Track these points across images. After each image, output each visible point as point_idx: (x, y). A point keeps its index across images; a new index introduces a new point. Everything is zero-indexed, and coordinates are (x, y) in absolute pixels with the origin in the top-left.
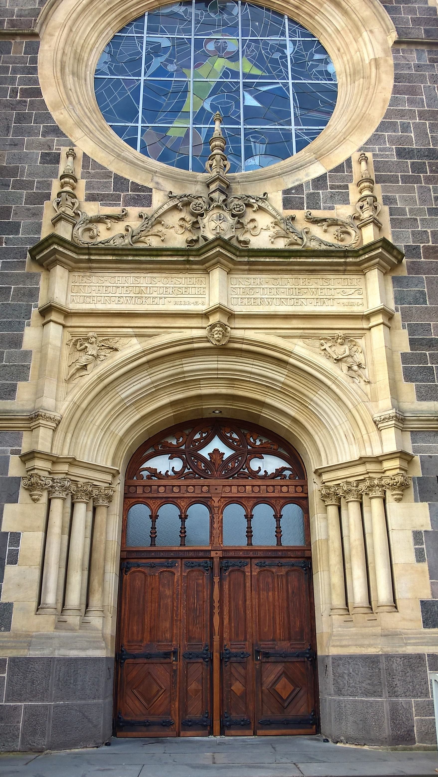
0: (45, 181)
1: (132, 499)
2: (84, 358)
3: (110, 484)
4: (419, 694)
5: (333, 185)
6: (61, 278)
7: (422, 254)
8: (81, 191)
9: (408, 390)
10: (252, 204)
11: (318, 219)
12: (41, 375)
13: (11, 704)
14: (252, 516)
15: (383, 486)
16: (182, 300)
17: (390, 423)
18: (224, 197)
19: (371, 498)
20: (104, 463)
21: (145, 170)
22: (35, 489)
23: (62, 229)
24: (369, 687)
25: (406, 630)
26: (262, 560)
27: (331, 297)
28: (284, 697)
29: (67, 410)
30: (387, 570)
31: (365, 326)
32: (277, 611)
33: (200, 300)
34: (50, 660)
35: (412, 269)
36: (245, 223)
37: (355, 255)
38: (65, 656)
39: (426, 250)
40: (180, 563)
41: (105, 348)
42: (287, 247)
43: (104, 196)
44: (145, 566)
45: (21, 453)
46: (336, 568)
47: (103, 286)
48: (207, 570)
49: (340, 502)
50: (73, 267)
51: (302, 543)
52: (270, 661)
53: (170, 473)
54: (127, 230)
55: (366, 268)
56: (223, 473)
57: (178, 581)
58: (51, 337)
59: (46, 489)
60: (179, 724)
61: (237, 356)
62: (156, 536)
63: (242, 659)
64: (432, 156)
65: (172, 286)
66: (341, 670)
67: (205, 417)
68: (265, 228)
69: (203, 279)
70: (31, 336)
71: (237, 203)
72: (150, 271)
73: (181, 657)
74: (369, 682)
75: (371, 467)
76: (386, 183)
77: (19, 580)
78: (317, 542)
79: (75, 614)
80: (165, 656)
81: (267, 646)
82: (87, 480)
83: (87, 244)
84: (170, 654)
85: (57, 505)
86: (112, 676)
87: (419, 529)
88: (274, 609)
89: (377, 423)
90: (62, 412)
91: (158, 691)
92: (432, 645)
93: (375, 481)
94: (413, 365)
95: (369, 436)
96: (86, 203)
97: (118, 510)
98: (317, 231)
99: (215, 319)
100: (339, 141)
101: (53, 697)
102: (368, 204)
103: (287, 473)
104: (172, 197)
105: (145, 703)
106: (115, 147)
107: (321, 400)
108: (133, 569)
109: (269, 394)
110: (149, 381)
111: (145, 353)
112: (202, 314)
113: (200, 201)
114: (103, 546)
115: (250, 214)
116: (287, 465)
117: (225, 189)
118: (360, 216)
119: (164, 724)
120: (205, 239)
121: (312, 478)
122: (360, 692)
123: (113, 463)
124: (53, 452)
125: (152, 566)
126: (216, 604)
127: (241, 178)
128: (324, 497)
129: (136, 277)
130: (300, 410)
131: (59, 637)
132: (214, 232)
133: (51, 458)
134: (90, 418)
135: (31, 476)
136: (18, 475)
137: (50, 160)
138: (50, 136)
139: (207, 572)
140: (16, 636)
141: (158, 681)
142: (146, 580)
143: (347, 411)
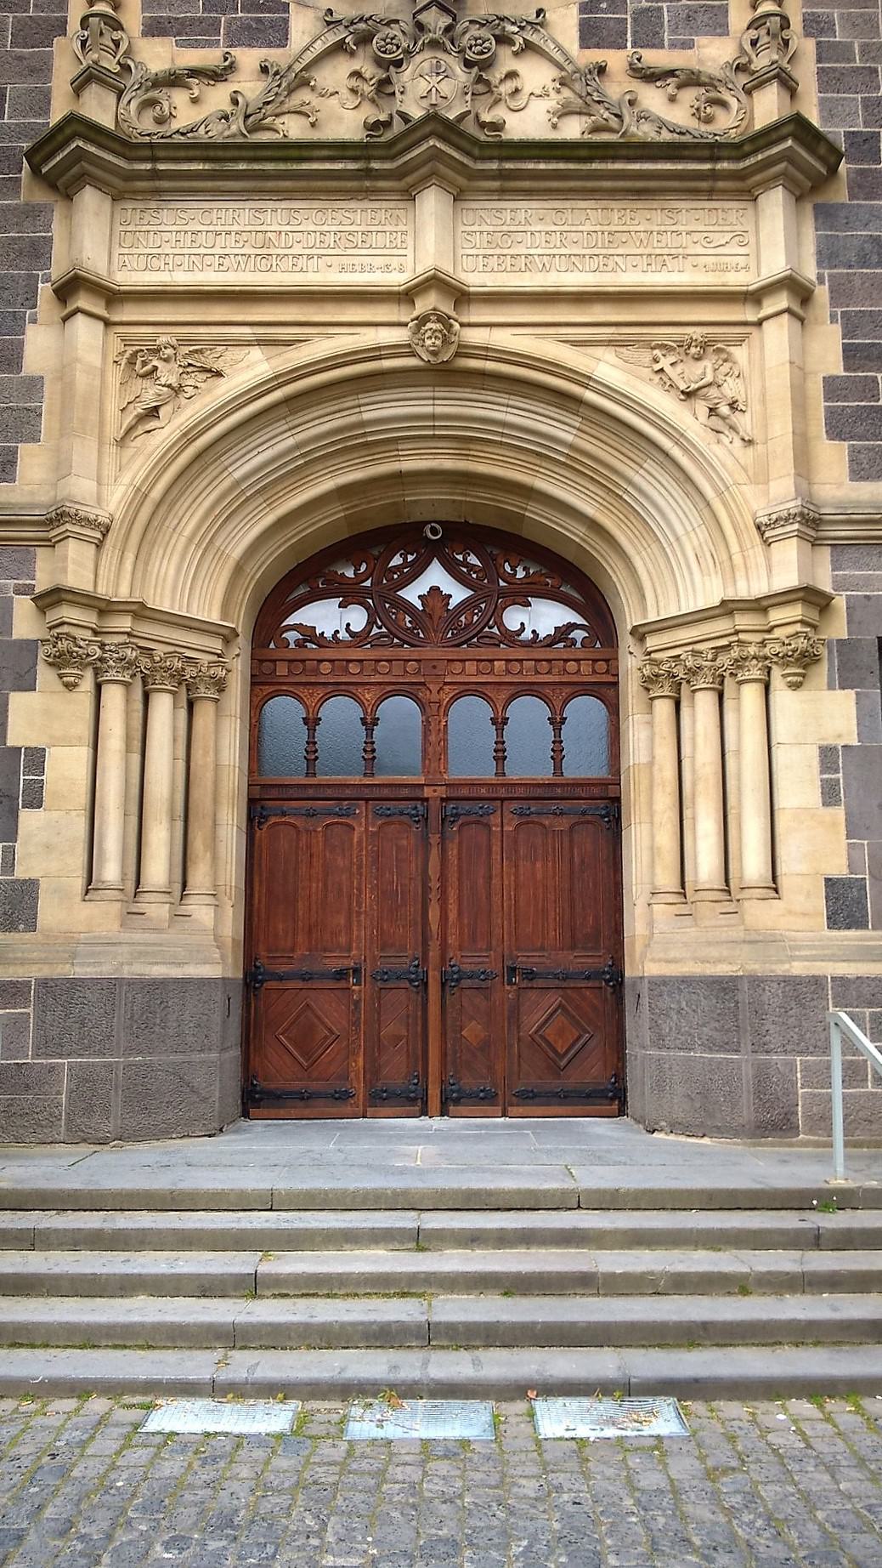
9: (833, 458)
14: (505, 721)
15: (766, 658)
16: (356, 260)
17: (789, 528)
22: (67, 664)
23: (94, 103)
24: (715, 1034)
26: (525, 805)
31: (751, 316)
33: (395, 262)
35: (860, 187)
37: (734, 153)
42: (586, 136)
43: (182, 24)
49: (679, 691)
50: (121, 191)
53: (343, 635)
54: (235, 102)
55: (759, 184)
57: (360, 842)
65: (334, 228)
66: (666, 1002)
68: (538, 92)
70: (40, 344)
71: (477, 33)
72: (286, 195)
75: (743, 621)
77: (45, 842)
82: (171, 649)
85: (114, 697)
87: (831, 742)
90: (111, 508)
98: (653, 99)
103: (579, 635)
107: (650, 481)
108: (273, 820)
110: (291, 442)
111: (279, 380)
112: (399, 293)
113: (394, 31)
114: (210, 775)
115: (506, 61)
116: (578, 619)
118: (750, 62)
120: (405, 118)
121: (626, 642)
123: (225, 614)
126: (434, 884)
128: (649, 682)
132: (425, 103)
133: (96, 603)
142: (298, 839)
143: (702, 505)
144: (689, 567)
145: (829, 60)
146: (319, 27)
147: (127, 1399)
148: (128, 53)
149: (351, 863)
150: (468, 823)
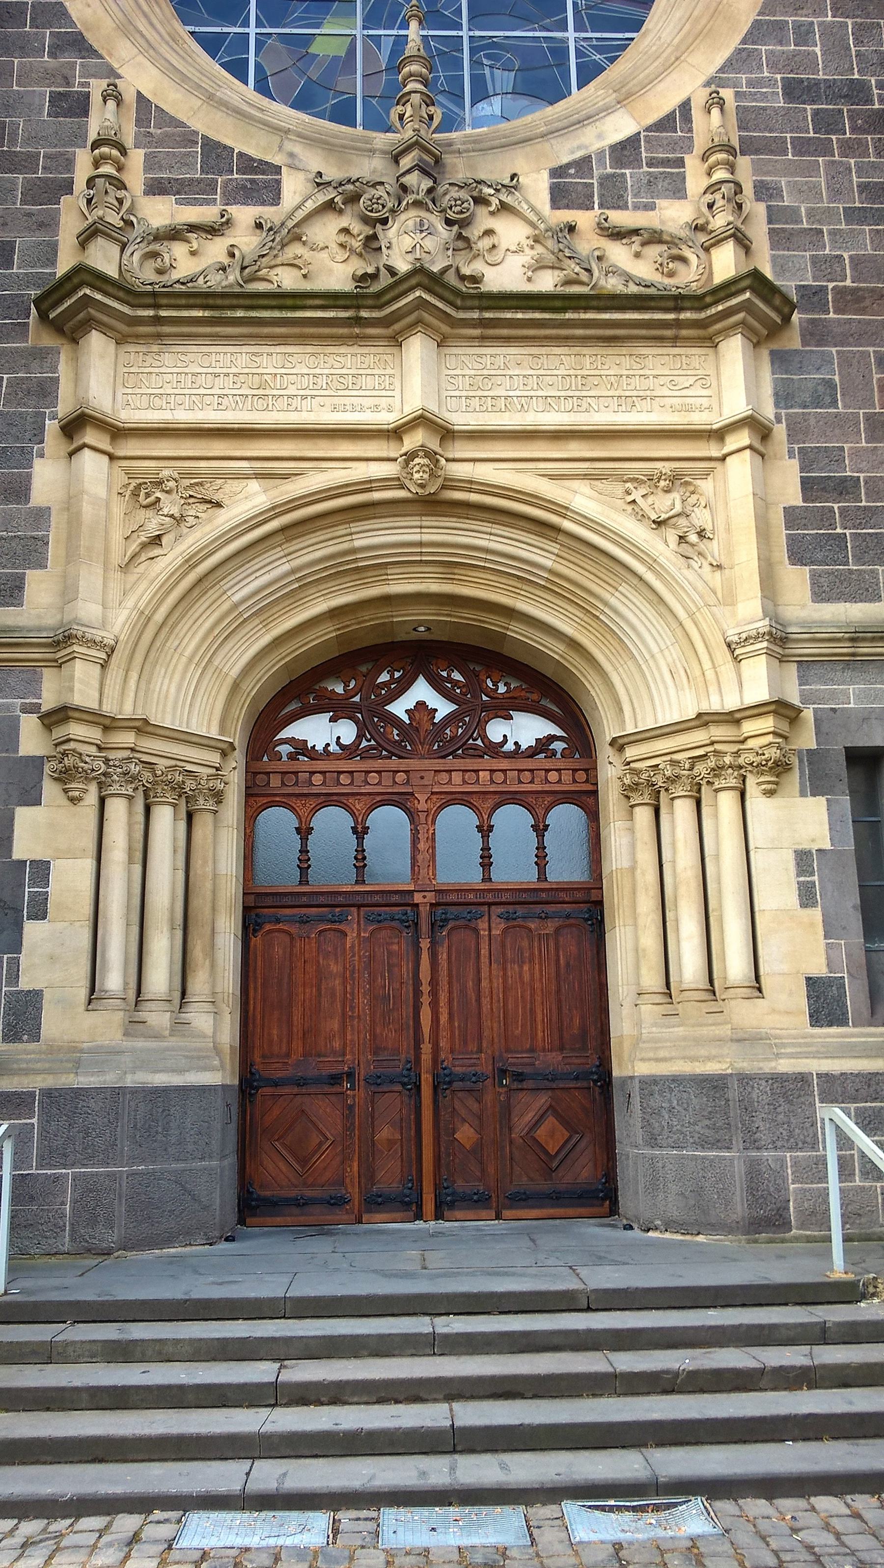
0: (62, 154)
1: (261, 798)
2: (154, 521)
3: (217, 769)
4: (800, 1145)
5: (654, 158)
6: (102, 357)
7: (831, 304)
8: (136, 176)
9: (796, 581)
10: (487, 197)
11: (622, 230)
12: (71, 555)
13: (49, 1172)
14: (491, 828)
15: (741, 767)
16: (347, 401)
18: (430, 183)
19: (717, 791)
20: (184, 725)
21: (267, 128)
23: (99, 254)
24: (707, 1132)
25: (778, 1031)
26: (511, 908)
27: (648, 393)
28: (552, 1149)
29: (127, 626)
30: (744, 921)
31: (715, 453)
32: (538, 999)
33: (384, 402)
34: (118, 1092)
35: (811, 334)
36: (473, 238)
37: (696, 305)
38: (145, 1083)
39: (839, 296)
40: (356, 914)
41: (196, 500)
42: (559, 289)
44: (290, 920)
45: (42, 710)
46: (649, 920)
47: (186, 374)
48: (407, 927)
49: (658, 799)
51: (586, 876)
52: (525, 1087)
53: (333, 748)
54: (233, 255)
55: (719, 332)
56: (436, 747)
57: (352, 947)
58: (86, 479)
59: (94, 778)
60: (360, 1201)
61: (460, 517)
62: (309, 866)
63: (473, 1084)
64: (857, 96)
65: (326, 371)
66: (656, 1101)
67: (399, 639)
68: (513, 248)
69: (389, 358)
70: (46, 477)
73: (362, 1083)
74: (707, 1122)
75: (718, 732)
76: (762, 154)
77: (48, 954)
78: (614, 875)
79: (159, 1009)
80: (332, 1081)
81: (520, 1060)
82: (173, 763)
83: (150, 284)
84: (341, 1078)
85: (117, 808)
86: (235, 1118)
87: (806, 846)
88: (532, 996)
89: (733, 646)
90: (116, 629)
91: (321, 1144)
92: (827, 1058)
93: (725, 759)
94: (806, 532)
95: (716, 673)
96: (147, 198)
97: (235, 819)
98: (619, 254)
99: (414, 440)
100: (667, 64)
101: (125, 1158)
102: (723, 197)
103: (559, 746)
104: (322, 184)
105: (296, 1166)
106: (204, 78)
107: (625, 605)
108: (268, 927)
109: (522, 593)
110: (286, 567)
111: (276, 511)
113: (380, 192)
114: (209, 885)
115: (483, 220)
117: (433, 166)
118: (707, 223)
119: (332, 1201)
120: (392, 271)
121: (605, 754)
122: (691, 1140)
123: (222, 730)
124: (104, 708)
125: (304, 921)
126: (425, 988)
127: (464, 143)
128: (628, 791)
129: (254, 354)
130: (582, 623)
131: (133, 1050)
132: (410, 258)
133: (101, 720)
134: (173, 643)
135: (64, 754)
136: (38, 753)
137: (70, 109)
138: (66, 54)
139: (406, 930)
140: (52, 1050)
141: (321, 1126)
142: (292, 946)
143: (674, 625)
144: (664, 682)
145: (778, 222)
146: (310, 188)
147: (158, 1515)
148: (130, 211)
149: (345, 968)
150: (459, 927)
